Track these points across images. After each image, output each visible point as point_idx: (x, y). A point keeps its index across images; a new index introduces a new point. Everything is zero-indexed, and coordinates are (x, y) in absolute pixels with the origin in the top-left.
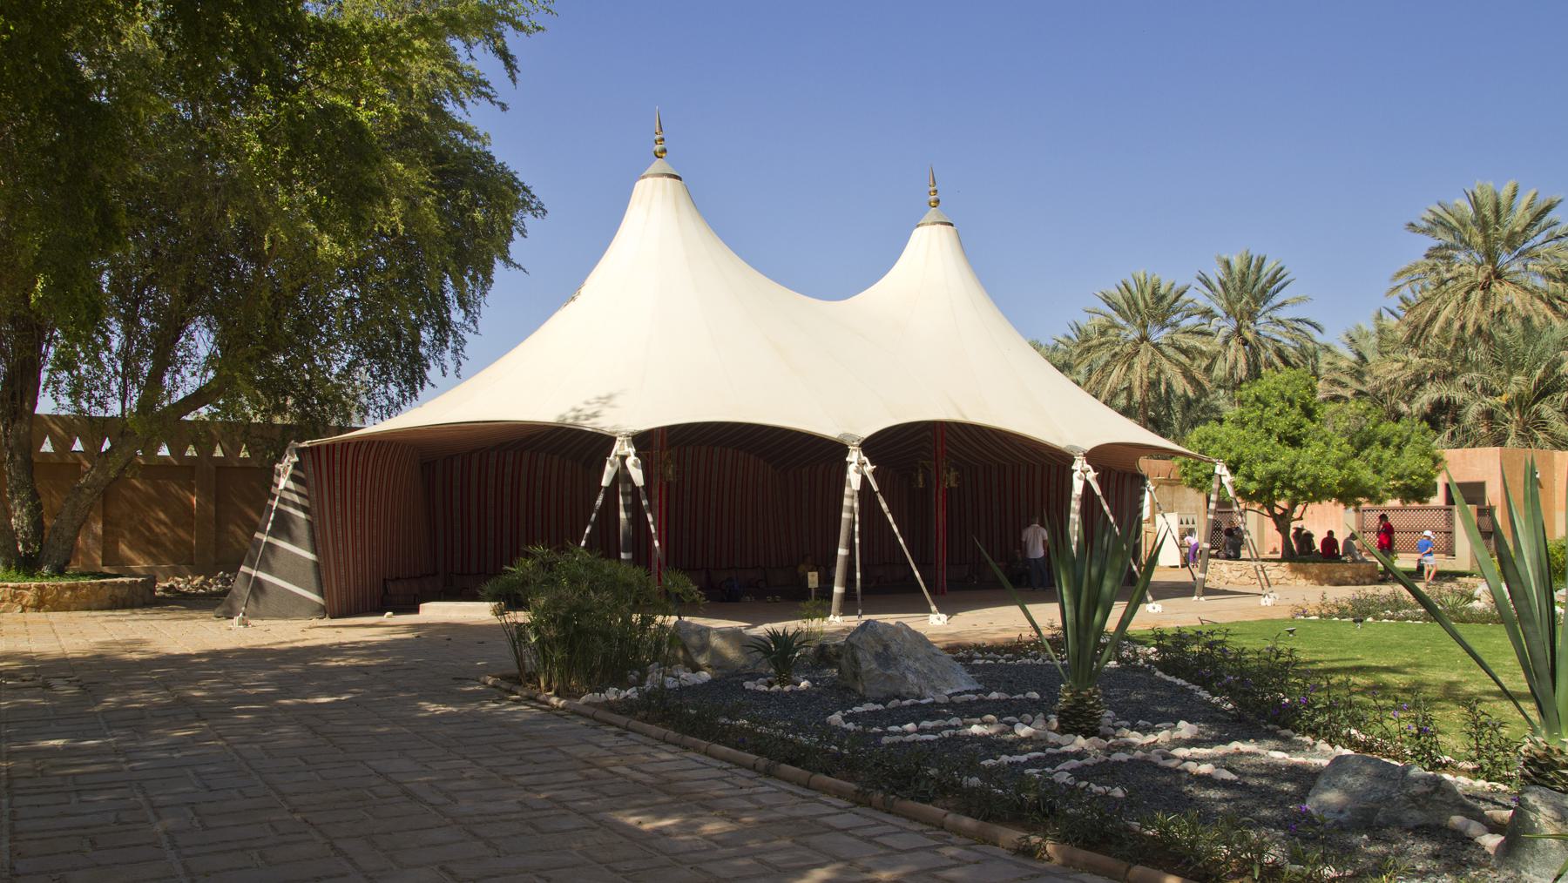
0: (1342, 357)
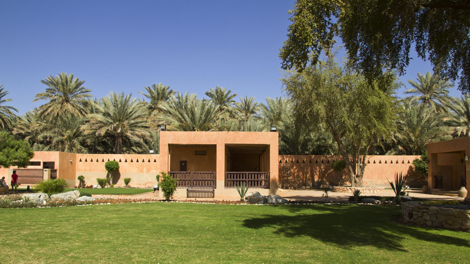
0: (23, 120)
